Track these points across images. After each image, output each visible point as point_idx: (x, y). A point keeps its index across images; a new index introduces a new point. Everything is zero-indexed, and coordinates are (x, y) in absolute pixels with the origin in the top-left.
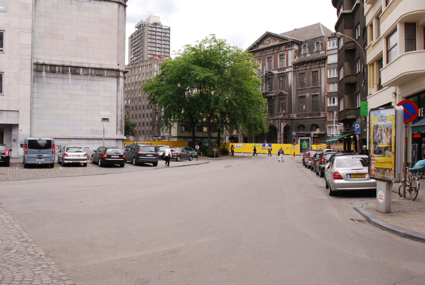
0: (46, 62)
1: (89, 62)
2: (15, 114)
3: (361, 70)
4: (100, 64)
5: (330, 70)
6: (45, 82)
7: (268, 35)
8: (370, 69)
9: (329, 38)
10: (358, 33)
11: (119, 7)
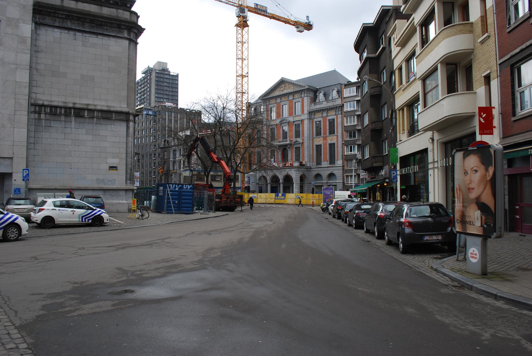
0: (46, 103)
1: (96, 103)
2: (8, 162)
3: (388, 115)
4: (108, 106)
5: (347, 118)
6: (44, 125)
7: (282, 82)
8: (399, 115)
9: (345, 85)
10: (385, 78)
11: (129, 44)
